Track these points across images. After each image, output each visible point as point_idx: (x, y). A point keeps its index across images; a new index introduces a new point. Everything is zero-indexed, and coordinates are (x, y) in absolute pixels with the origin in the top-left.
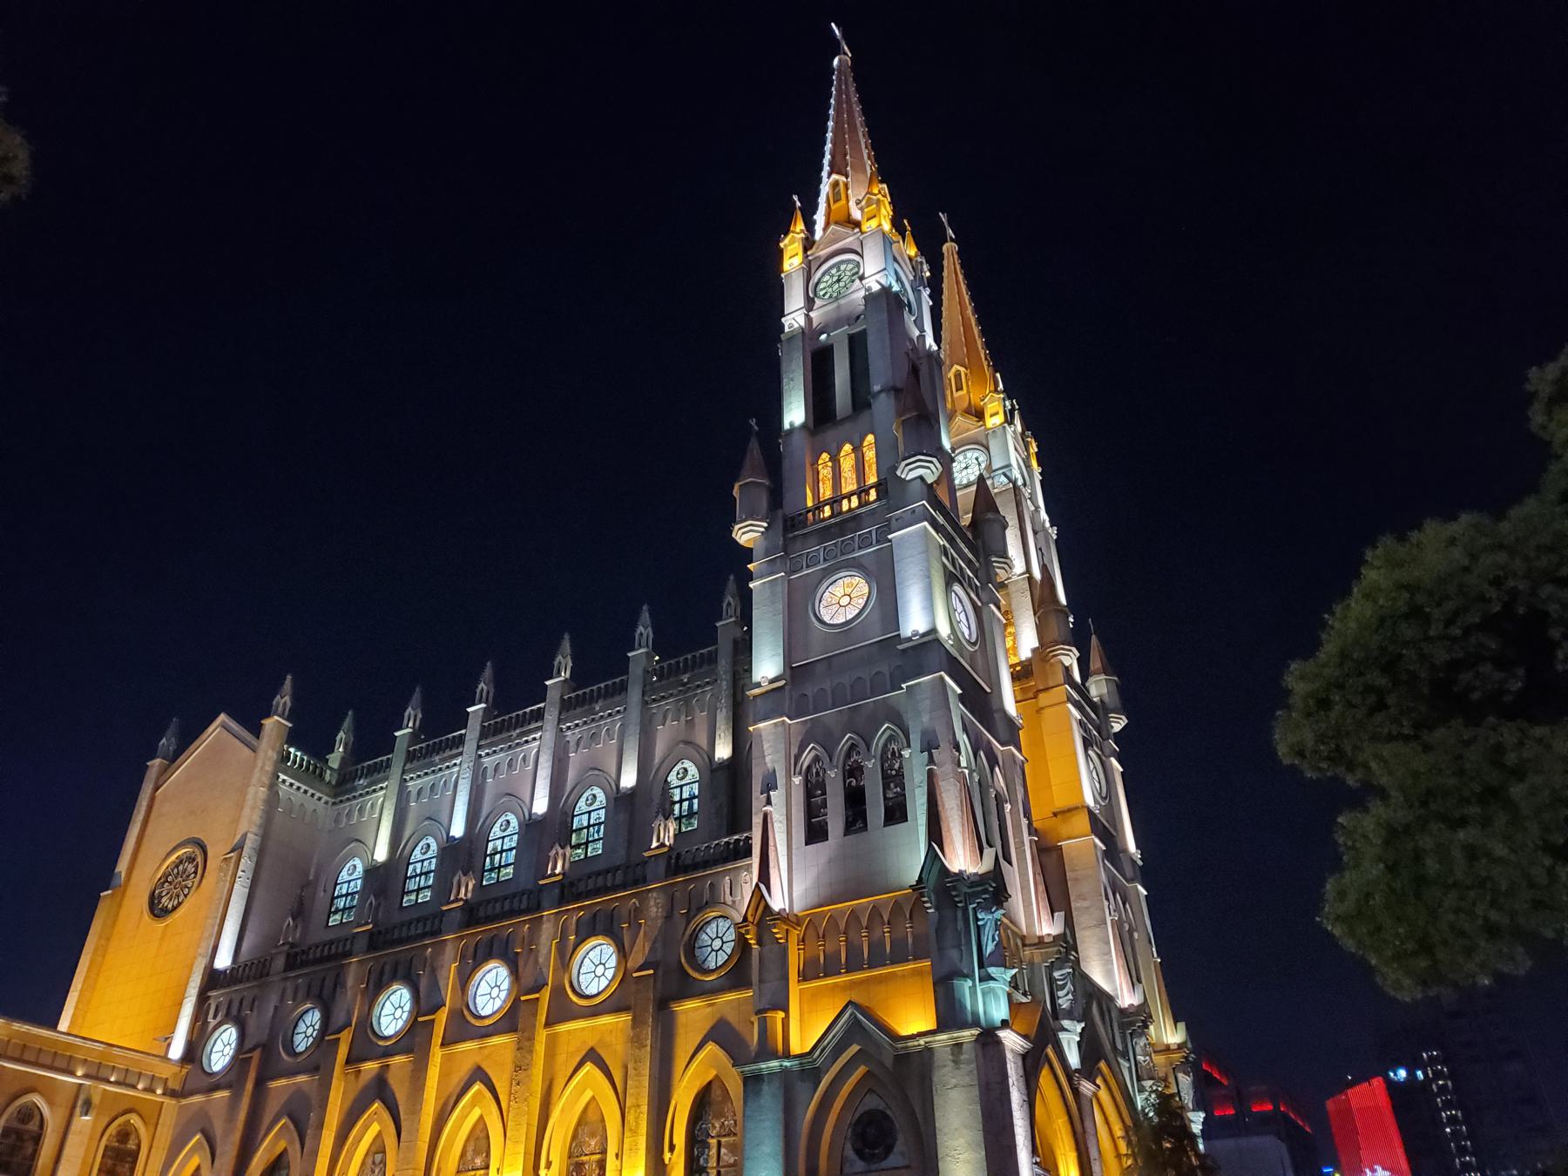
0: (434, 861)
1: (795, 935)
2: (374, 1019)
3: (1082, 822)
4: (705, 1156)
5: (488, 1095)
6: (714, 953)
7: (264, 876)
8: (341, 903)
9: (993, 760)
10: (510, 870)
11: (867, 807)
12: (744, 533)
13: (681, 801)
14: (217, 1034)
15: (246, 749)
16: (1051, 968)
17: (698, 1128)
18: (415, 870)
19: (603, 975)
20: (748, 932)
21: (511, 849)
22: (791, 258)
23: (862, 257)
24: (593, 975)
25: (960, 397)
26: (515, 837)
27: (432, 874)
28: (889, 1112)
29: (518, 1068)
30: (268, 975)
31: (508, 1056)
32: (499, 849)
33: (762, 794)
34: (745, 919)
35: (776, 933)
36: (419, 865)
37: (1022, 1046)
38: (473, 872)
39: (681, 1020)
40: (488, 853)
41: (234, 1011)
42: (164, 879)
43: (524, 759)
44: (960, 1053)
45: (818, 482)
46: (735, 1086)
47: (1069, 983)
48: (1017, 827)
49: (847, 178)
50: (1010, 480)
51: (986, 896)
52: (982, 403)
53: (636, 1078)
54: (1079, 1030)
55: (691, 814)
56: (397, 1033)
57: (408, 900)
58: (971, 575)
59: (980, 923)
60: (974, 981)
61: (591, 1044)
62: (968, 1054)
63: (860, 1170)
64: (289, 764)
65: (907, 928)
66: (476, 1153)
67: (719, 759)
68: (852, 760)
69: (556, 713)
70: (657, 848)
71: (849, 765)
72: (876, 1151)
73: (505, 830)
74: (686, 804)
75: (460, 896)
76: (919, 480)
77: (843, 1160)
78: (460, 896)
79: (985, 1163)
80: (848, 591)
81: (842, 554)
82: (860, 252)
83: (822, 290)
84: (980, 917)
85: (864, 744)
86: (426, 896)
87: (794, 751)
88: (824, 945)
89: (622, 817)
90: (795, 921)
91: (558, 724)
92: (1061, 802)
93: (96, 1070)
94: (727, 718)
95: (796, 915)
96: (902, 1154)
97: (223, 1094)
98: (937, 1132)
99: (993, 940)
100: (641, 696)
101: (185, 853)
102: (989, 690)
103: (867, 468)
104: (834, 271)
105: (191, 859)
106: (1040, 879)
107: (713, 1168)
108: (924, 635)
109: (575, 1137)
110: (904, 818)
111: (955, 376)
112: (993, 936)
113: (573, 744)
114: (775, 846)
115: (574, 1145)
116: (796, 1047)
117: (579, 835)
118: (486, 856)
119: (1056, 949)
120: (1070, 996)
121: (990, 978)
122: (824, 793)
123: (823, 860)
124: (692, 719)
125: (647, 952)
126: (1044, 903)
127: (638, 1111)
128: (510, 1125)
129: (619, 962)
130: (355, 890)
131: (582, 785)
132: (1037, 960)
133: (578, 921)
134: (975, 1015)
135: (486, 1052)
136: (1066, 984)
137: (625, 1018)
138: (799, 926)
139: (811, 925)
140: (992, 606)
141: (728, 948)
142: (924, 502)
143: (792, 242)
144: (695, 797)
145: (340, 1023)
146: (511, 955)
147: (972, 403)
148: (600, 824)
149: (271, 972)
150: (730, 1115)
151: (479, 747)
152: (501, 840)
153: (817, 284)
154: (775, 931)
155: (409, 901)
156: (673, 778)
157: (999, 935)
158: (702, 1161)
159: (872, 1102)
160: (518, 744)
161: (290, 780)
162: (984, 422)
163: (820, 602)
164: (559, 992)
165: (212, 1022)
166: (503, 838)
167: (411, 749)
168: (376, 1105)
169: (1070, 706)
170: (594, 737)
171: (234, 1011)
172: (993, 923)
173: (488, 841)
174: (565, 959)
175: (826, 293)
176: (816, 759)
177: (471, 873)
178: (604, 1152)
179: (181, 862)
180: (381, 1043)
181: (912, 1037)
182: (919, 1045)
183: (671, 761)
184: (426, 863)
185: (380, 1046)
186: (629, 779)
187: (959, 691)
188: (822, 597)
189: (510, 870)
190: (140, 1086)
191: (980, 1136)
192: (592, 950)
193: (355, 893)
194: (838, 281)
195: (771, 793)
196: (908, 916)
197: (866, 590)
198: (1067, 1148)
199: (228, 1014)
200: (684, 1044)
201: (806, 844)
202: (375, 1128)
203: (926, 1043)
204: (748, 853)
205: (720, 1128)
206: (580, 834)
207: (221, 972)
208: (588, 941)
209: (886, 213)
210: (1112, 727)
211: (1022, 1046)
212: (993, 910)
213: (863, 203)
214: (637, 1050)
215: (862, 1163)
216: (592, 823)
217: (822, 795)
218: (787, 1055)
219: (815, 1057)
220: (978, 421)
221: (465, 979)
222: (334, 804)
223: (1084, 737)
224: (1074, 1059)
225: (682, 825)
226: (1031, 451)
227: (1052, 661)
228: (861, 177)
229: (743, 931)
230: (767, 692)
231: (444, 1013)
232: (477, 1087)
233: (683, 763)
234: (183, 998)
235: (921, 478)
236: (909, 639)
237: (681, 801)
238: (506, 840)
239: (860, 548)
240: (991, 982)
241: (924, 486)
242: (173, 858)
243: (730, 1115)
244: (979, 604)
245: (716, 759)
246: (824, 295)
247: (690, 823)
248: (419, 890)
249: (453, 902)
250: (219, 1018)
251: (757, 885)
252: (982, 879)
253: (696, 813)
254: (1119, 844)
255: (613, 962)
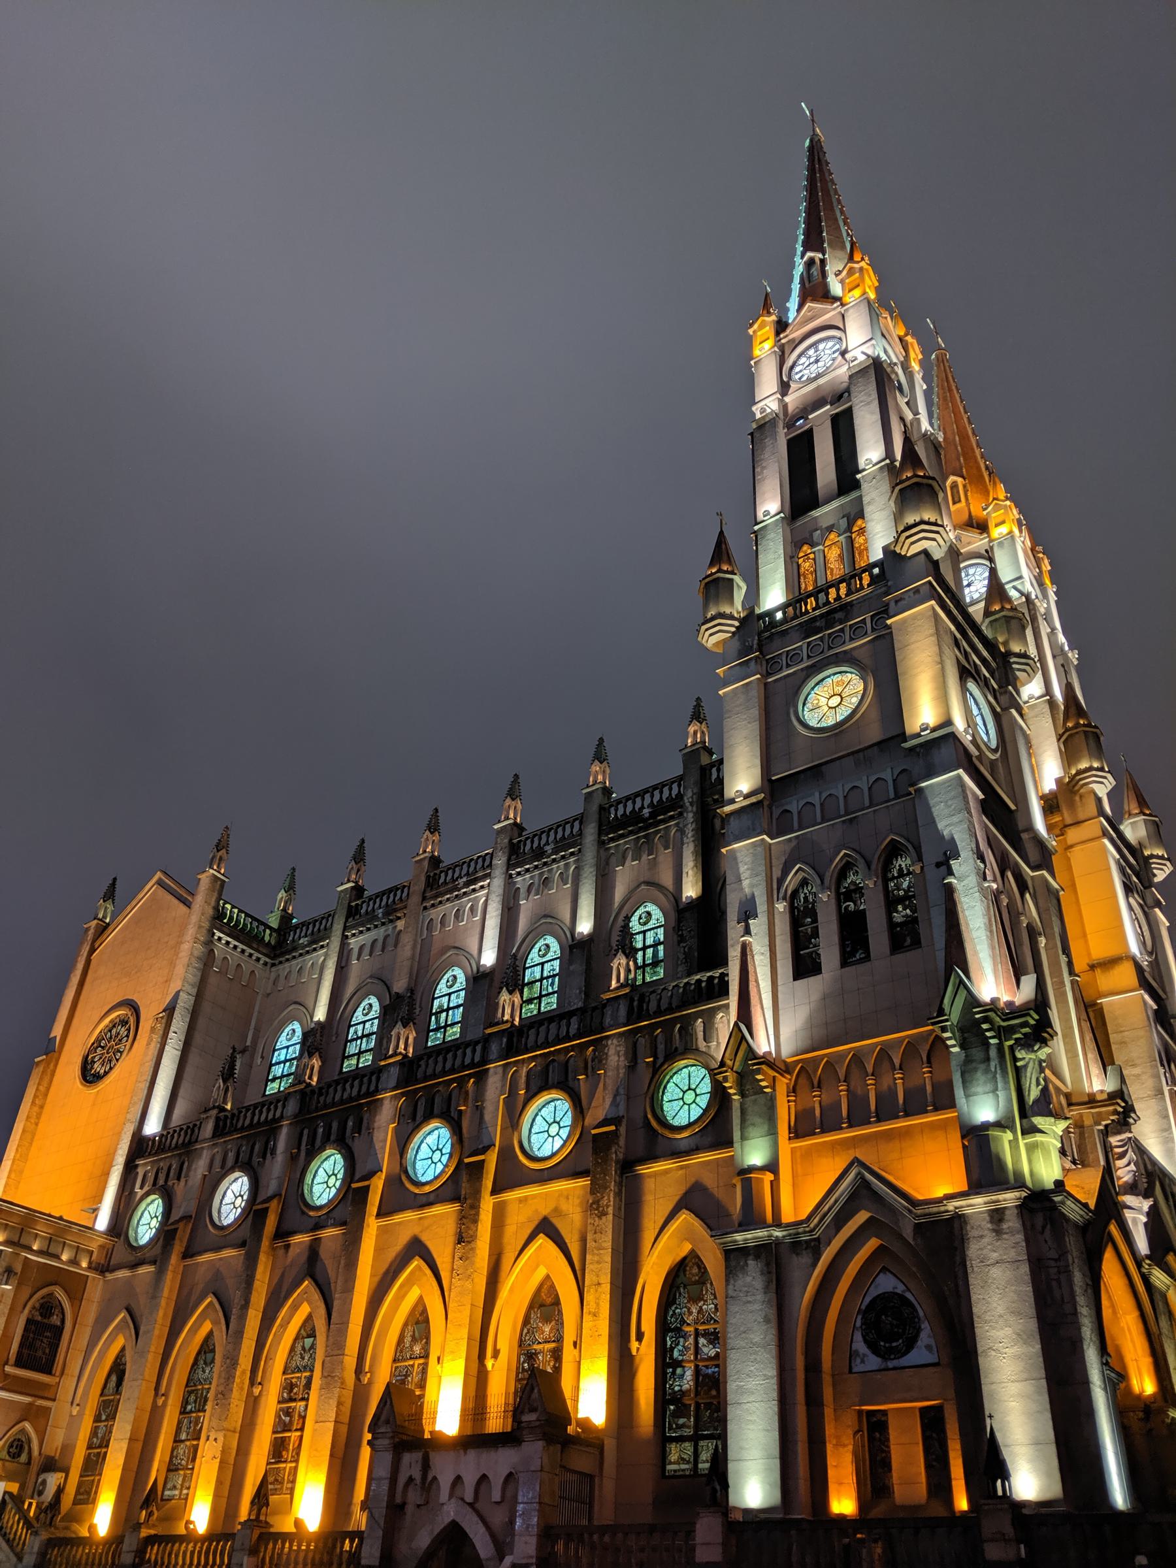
0: (376, 1022)
1: (783, 1083)
2: (306, 1187)
3: (1125, 975)
4: (680, 1348)
5: (428, 1272)
6: (686, 1107)
7: (198, 1038)
8: (277, 1071)
9: (1022, 886)
10: (457, 1029)
11: (869, 933)
12: (711, 635)
13: (644, 948)
14: (143, 1205)
15: (182, 906)
16: (1106, 1132)
17: (671, 1313)
18: (356, 1032)
19: (558, 1134)
20: (726, 1079)
21: (458, 1007)
22: (761, 343)
23: (844, 331)
24: (546, 1135)
25: (958, 511)
26: (463, 994)
27: (374, 1037)
28: (908, 1295)
29: (460, 1239)
30: (196, 1141)
31: (449, 1228)
32: (445, 1007)
33: (739, 923)
34: (722, 1064)
35: (762, 1080)
36: (360, 1027)
37: (1081, 1216)
38: (414, 1024)
39: (649, 1185)
40: (434, 1011)
41: (161, 1182)
42: (97, 1044)
43: (472, 909)
44: (1001, 1220)
45: (799, 578)
46: (713, 1262)
47: (1130, 1150)
48: (1055, 965)
49: (824, 255)
50: (1022, 594)
51: (1027, 1030)
52: (985, 513)
53: (596, 1252)
54: (1146, 1208)
55: (655, 963)
56: (330, 1201)
57: (349, 1065)
58: (987, 675)
59: (1019, 1064)
60: (1014, 1132)
61: (545, 1211)
62: (1012, 1222)
63: (875, 1368)
64: (225, 921)
65: (924, 1073)
66: (414, 1340)
67: (687, 897)
68: (849, 881)
69: (504, 859)
70: (617, 989)
71: (845, 888)
72: (894, 1344)
73: (451, 986)
74: (650, 952)
75: (399, 1051)
76: (923, 556)
77: (853, 1355)
78: (399, 1051)
79: (1041, 1359)
80: (838, 689)
81: (830, 648)
82: (841, 326)
83: (797, 373)
84: (1019, 1055)
85: (862, 861)
86: (367, 1060)
87: (777, 873)
88: (820, 1096)
89: (578, 967)
90: (783, 1068)
91: (507, 870)
92: (1099, 949)
93: (18, 1235)
94: (695, 853)
95: (784, 1062)
96: (928, 1347)
97: (146, 1270)
98: (975, 1319)
99: (1038, 1084)
100: (597, 836)
101: (119, 1016)
102: (1013, 807)
103: (857, 555)
104: (811, 352)
105: (124, 1022)
106: (1086, 1025)
107: (690, 1361)
108: (934, 730)
109: (526, 1321)
110: (917, 943)
111: (952, 488)
112: (1038, 1080)
113: (523, 891)
114: (757, 981)
115: (525, 1331)
116: (788, 1216)
117: (530, 989)
118: (431, 1014)
119: (1111, 1108)
120: (1132, 1167)
121: (1035, 1130)
122: (815, 921)
123: (816, 996)
124: (654, 858)
125: (607, 1106)
126: (1093, 1055)
127: (599, 1290)
128: (451, 1306)
129: (575, 1120)
130: (294, 1056)
131: (534, 934)
132: (1088, 1122)
133: (528, 1073)
134: (1019, 1176)
135: (426, 1223)
136: (1125, 1153)
137: (583, 1183)
138: (789, 1073)
139: (803, 1075)
140: (1013, 711)
141: (703, 1101)
142: (930, 578)
143: (761, 327)
144: (660, 943)
145: (270, 1192)
146: (454, 1114)
147: (973, 514)
148: (554, 976)
149: (200, 1139)
150: (709, 1297)
151: (424, 899)
152: (447, 997)
153: (792, 368)
154: (759, 1077)
155: (349, 1065)
156: (635, 925)
157: (1045, 1079)
158: (676, 1354)
159: (887, 1283)
160: (465, 893)
161: (225, 938)
162: (988, 533)
163: (804, 704)
164: (506, 1155)
165: (139, 1192)
166: (449, 994)
167: (353, 904)
168: (306, 1282)
169: (1106, 842)
170: (546, 882)
171: (161, 1182)
172: (1037, 1063)
173: (434, 999)
174: (513, 1119)
175: (803, 376)
176: (804, 883)
177: (411, 1024)
178: (559, 1339)
179: (114, 1026)
180: (311, 1213)
181: (939, 1201)
182: (947, 1211)
183: (633, 900)
184: (368, 1025)
185: (310, 1216)
186: (585, 926)
187: (982, 796)
188: (806, 699)
189: (457, 1029)
190: (64, 1257)
191: (1033, 1325)
192: (544, 1106)
193: (293, 1059)
194: (817, 361)
195: (751, 922)
196: (925, 1059)
197: (861, 687)
198: (1140, 1352)
199: (154, 1184)
200: (655, 1209)
201: (794, 980)
202: (305, 1310)
203: (956, 1208)
204: (724, 991)
205: (699, 1312)
206: (532, 988)
207: (150, 1139)
208: (539, 1096)
209: (871, 283)
210: (1155, 875)
211: (1081, 1216)
212: (1036, 1048)
213: (844, 273)
214: (597, 1219)
215: (879, 1360)
216: (545, 975)
217: (813, 922)
218: (777, 1223)
219: (812, 1226)
220: (981, 533)
221: (403, 1143)
222: (273, 965)
223: (1124, 882)
224: (1142, 1245)
225: (646, 974)
226: (1044, 568)
227: (1082, 791)
228: (840, 254)
229: (720, 1077)
230: (743, 808)
231: (380, 1178)
232: (416, 1262)
233: (645, 907)
234: (111, 1166)
235: (925, 552)
236: (918, 735)
237: (644, 948)
238: (453, 997)
239: (852, 639)
240: (1037, 1134)
241: (929, 563)
242: (107, 1021)
243: (709, 1297)
244: (998, 709)
245: (684, 899)
246: (800, 378)
247: (655, 972)
248: (360, 1053)
249: (391, 1056)
250: (146, 1188)
251: (736, 1024)
252: (1013, 1011)
253: (662, 961)
254: (1169, 1010)
255: (568, 1121)
